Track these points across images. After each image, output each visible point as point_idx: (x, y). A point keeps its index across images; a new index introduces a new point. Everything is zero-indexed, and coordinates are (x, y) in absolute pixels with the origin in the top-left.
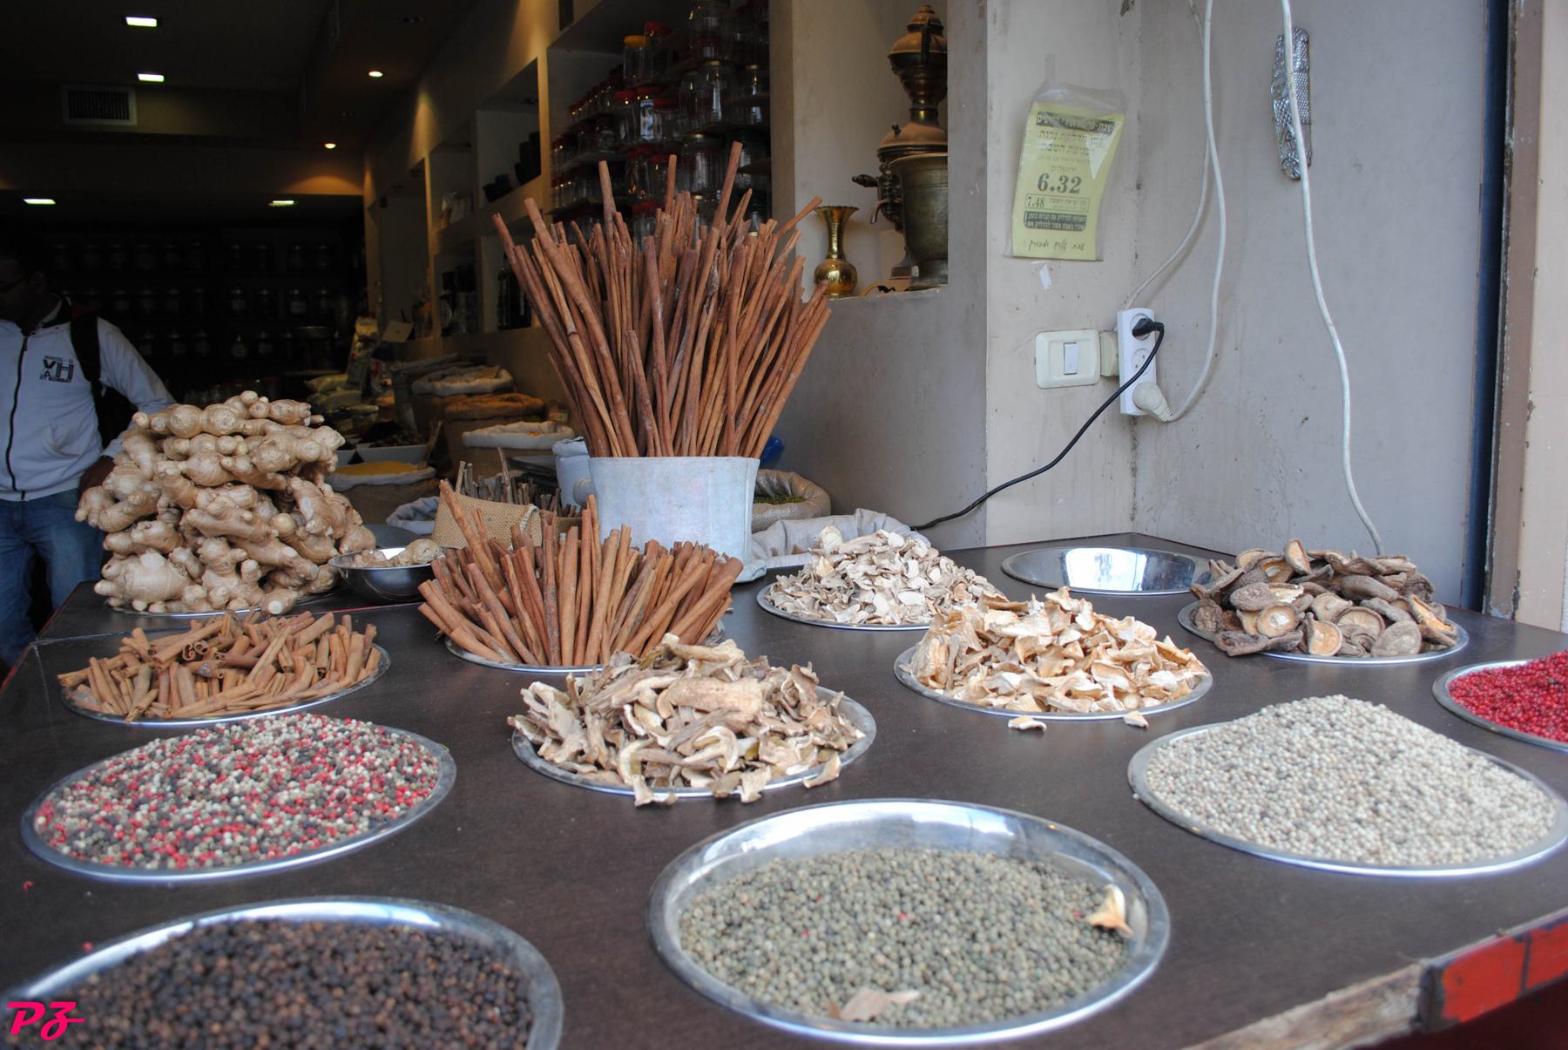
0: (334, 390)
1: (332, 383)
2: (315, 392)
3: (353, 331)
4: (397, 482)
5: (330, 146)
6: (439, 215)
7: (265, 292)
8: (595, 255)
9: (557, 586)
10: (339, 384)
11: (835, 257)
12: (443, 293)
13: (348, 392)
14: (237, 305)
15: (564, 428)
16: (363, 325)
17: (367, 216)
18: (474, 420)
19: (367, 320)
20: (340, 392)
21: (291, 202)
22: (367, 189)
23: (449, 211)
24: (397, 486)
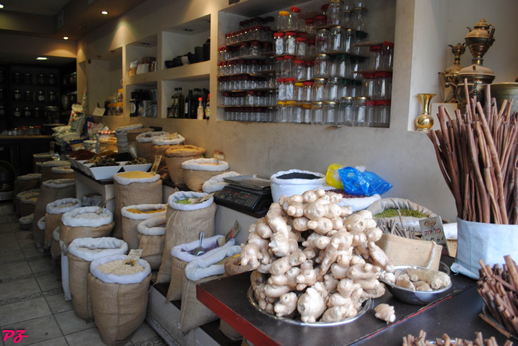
0: (65, 132)
1: (64, 129)
2: (57, 132)
3: (71, 109)
4: (149, 181)
5: (66, 38)
6: (129, 69)
7: (28, 92)
8: (453, 127)
9: (469, 289)
10: (67, 130)
11: (426, 114)
12: (131, 100)
13: (71, 133)
14: (17, 96)
15: (223, 162)
16: (75, 107)
17: (78, 67)
18: (182, 157)
19: (77, 105)
20: (68, 133)
21: (45, 59)
22: (80, 55)
23: (136, 69)
24: (148, 183)
